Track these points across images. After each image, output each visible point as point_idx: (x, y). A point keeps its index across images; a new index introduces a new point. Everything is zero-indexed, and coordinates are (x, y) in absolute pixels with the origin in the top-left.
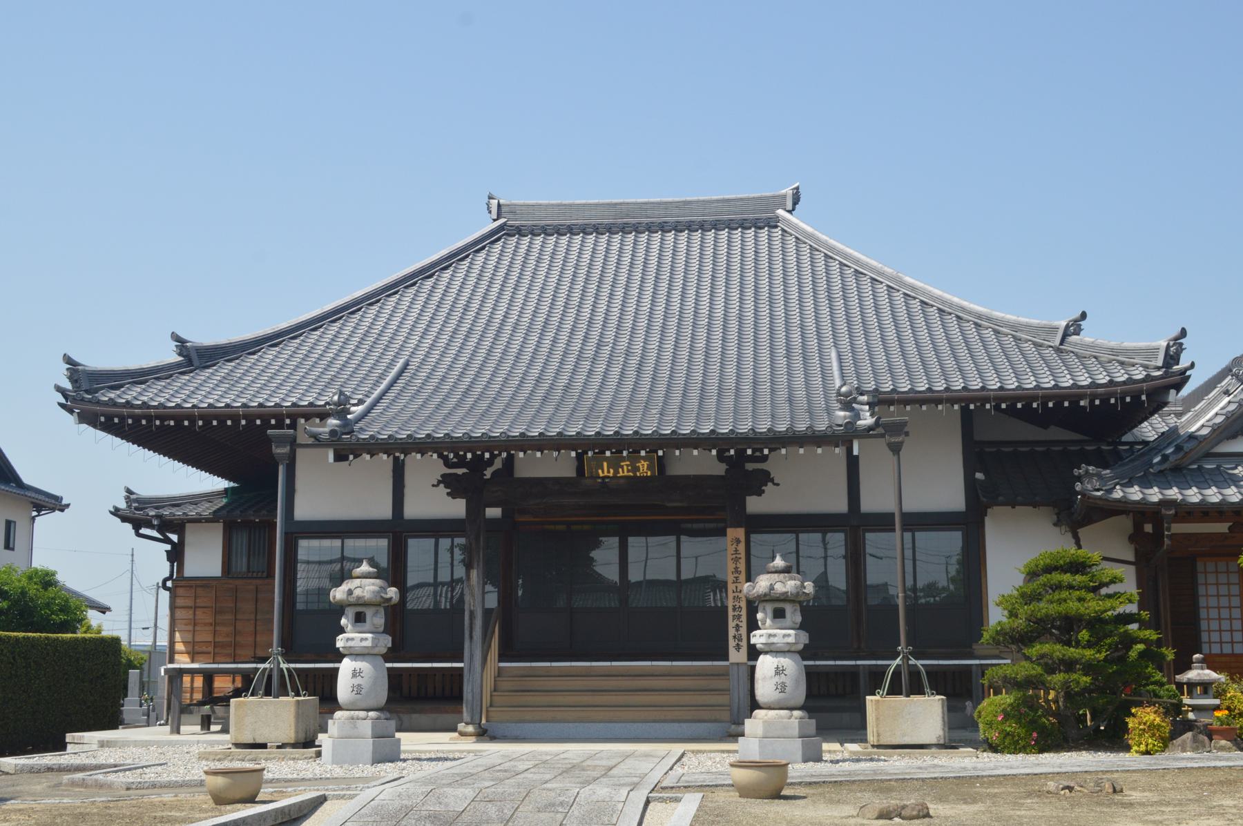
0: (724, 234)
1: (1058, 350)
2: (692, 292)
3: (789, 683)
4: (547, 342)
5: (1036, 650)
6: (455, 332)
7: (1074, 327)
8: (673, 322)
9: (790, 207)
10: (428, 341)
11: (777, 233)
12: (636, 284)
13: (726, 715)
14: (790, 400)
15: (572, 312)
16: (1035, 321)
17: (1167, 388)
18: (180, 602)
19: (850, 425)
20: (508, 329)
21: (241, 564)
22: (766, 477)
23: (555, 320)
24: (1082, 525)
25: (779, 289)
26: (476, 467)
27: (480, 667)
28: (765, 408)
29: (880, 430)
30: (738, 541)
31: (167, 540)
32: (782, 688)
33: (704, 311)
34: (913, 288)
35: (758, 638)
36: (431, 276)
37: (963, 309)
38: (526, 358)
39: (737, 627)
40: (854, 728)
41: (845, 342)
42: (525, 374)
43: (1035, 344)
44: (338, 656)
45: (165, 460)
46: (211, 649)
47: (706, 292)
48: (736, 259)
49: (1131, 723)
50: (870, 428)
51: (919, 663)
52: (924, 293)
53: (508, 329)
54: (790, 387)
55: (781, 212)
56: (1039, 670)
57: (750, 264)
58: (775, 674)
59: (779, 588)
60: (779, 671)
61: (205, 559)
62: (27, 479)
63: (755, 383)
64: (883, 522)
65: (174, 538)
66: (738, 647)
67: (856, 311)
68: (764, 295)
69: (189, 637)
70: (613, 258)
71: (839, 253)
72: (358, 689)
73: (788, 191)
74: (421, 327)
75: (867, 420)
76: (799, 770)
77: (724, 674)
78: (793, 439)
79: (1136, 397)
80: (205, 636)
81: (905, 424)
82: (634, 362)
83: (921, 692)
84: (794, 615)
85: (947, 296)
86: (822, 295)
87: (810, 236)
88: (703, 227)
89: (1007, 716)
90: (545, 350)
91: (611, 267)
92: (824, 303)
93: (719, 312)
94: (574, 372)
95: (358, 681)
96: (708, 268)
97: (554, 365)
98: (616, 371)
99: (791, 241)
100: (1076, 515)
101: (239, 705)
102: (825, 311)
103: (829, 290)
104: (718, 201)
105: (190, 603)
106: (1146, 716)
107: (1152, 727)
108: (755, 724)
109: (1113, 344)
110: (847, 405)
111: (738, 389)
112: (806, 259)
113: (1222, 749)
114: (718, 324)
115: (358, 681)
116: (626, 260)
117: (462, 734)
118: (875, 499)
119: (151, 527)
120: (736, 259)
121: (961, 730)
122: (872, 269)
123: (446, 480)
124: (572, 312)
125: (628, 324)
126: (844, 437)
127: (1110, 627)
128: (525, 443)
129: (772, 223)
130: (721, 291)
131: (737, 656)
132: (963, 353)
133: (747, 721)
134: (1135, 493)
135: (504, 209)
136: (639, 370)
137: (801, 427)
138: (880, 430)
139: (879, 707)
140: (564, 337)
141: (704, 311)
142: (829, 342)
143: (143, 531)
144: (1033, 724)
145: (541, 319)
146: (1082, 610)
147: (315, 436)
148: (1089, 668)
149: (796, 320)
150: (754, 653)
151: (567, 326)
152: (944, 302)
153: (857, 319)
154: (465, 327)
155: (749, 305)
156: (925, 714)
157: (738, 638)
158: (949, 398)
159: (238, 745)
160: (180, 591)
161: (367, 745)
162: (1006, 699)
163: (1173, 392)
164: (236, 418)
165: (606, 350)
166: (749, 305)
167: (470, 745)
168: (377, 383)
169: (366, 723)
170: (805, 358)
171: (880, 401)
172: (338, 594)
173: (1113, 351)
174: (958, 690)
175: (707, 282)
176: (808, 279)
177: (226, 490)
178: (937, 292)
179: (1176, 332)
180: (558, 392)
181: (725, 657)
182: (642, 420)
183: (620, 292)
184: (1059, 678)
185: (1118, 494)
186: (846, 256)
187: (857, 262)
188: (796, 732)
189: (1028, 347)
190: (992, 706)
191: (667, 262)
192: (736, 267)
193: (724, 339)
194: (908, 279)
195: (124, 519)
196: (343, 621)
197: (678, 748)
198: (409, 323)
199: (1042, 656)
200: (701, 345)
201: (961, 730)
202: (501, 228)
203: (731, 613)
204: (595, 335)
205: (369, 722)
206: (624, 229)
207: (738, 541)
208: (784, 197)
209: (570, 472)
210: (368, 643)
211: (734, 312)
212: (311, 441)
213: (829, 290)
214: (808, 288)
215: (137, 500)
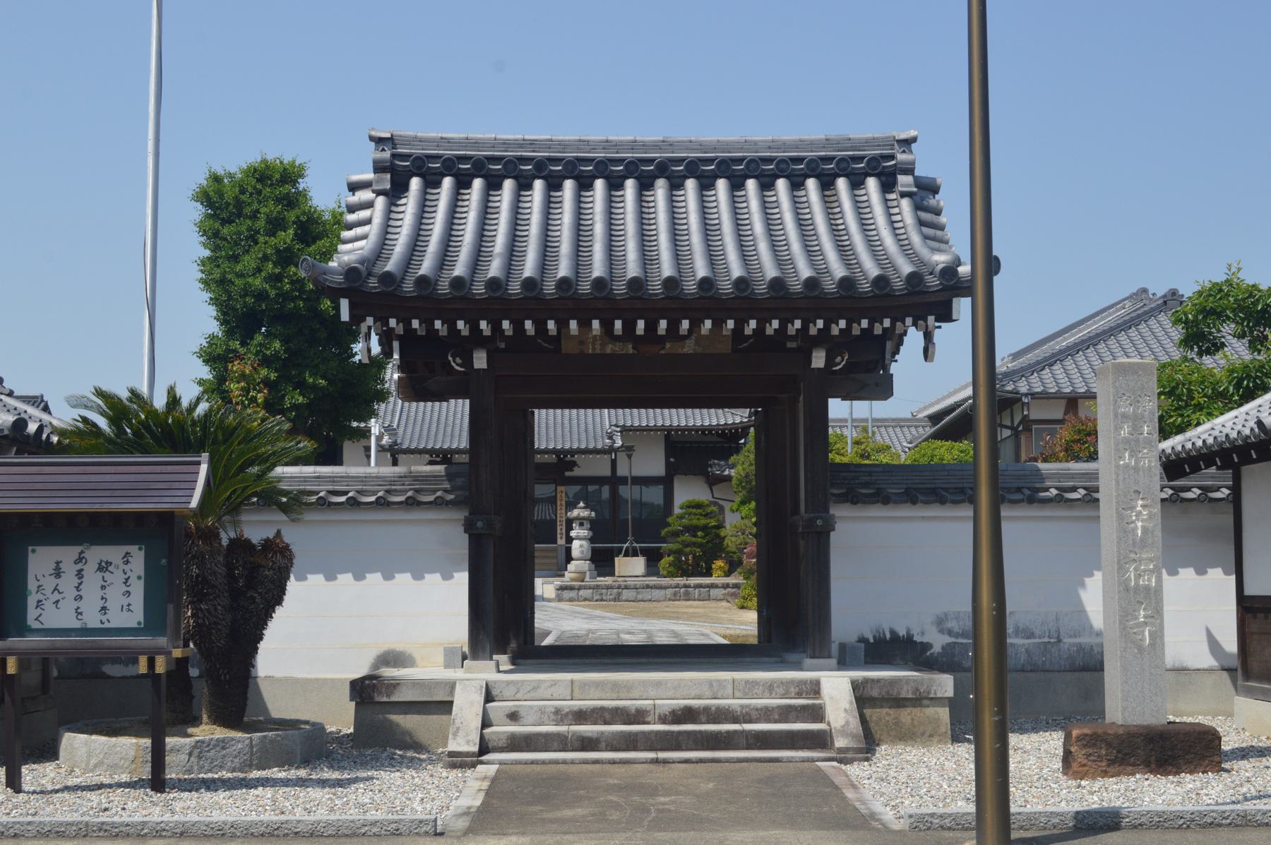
14: (586, 431)
19: (611, 447)
22: (574, 464)
28: (575, 436)
32: (582, 552)
64: (623, 480)
75: (619, 443)
76: (587, 579)
77: (555, 550)
79: (737, 430)
84: (587, 525)
100: (714, 481)
110: (610, 438)
118: (622, 471)
121: (652, 569)
126: (611, 450)
131: (561, 541)
137: (591, 446)
144: (679, 568)
148: (700, 545)
158: (656, 429)
174: (653, 559)
184: (688, 549)
185: (726, 473)
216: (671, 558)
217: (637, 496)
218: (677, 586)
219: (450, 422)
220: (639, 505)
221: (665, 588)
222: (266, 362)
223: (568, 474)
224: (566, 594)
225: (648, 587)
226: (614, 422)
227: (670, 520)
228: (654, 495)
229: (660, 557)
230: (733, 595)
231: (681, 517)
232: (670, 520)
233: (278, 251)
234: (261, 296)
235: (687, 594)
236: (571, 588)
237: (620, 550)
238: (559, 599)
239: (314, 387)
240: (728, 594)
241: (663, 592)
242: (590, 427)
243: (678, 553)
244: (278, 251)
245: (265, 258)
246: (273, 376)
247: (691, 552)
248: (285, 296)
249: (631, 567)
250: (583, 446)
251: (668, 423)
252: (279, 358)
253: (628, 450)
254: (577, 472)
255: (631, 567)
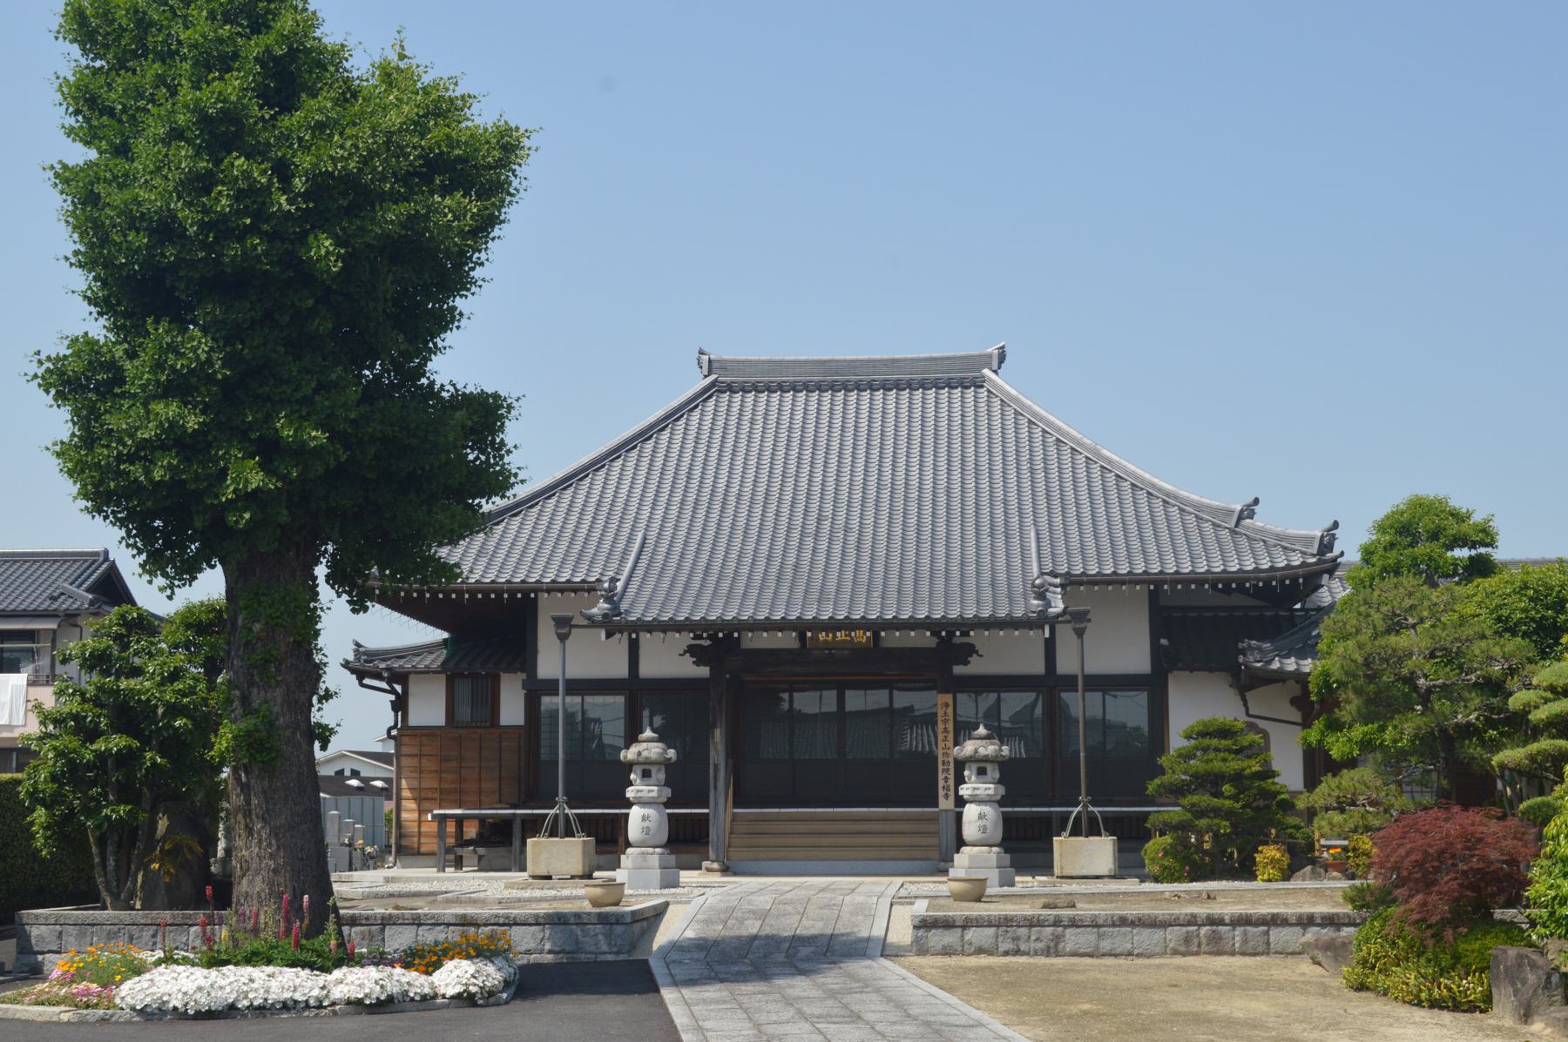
0: (931, 393)
1: (1233, 532)
2: (902, 460)
3: (989, 824)
4: (771, 515)
5: (1185, 801)
6: (683, 502)
7: (1248, 511)
8: (886, 494)
9: (995, 367)
10: (659, 513)
11: (983, 393)
12: (848, 451)
13: (935, 854)
14: (993, 584)
15: (790, 482)
16: (1215, 503)
17: (1320, 574)
18: (405, 750)
20: (732, 499)
21: (465, 712)
22: (970, 650)
23: (775, 489)
24: (1251, 688)
25: (984, 459)
26: (718, 643)
27: (721, 811)
29: (1068, 617)
30: (947, 705)
31: (393, 691)
32: (984, 829)
33: (914, 483)
34: (1110, 461)
35: (965, 791)
36: (649, 438)
37: (1154, 486)
38: (754, 532)
39: (946, 779)
40: (1046, 867)
41: (1043, 519)
42: (756, 550)
43: (1214, 524)
44: (629, 804)
45: (414, 622)
46: (436, 795)
47: (915, 460)
48: (944, 423)
49: (1258, 857)
50: (1058, 615)
51: (1095, 809)
52: (1120, 467)
53: (732, 499)
54: (993, 570)
55: (986, 372)
56: (1189, 815)
57: (957, 430)
58: (977, 819)
59: (982, 751)
60: (981, 816)
61: (429, 710)
62: (140, 604)
63: (962, 564)
64: (1069, 682)
65: (398, 688)
66: (947, 796)
67: (1055, 484)
68: (971, 466)
69: (415, 784)
70: (825, 420)
71: (1042, 419)
72: (647, 830)
73: (992, 350)
74: (650, 496)
75: (1058, 606)
76: (993, 889)
77: (934, 819)
78: (993, 624)
79: (1294, 580)
80: (430, 782)
81: (1086, 613)
82: (853, 538)
83: (1099, 834)
84: (993, 772)
85: (1140, 472)
86: (1025, 467)
87: (1016, 400)
88: (911, 386)
89: (1166, 853)
90: (769, 524)
91: (824, 431)
92: (1026, 475)
93: (928, 485)
94: (800, 549)
95: (647, 824)
96: (917, 433)
97: (780, 543)
98: (837, 547)
99: (996, 403)
100: (1247, 682)
101: (535, 844)
102: (1027, 484)
103: (1031, 460)
104: (925, 359)
105: (415, 751)
106: (1269, 853)
107: (1273, 860)
108: (963, 859)
109: (1279, 529)
110: (1041, 596)
111: (947, 571)
112: (1010, 424)
113: (1334, 878)
114: (928, 496)
115: (647, 824)
116: (838, 422)
117: (709, 870)
118: (1067, 664)
119: (378, 676)
120: (944, 423)
121: (1129, 865)
122: (1073, 439)
123: (692, 650)
124: (790, 482)
125: (844, 497)
127: (1247, 782)
128: (755, 626)
129: (978, 384)
130: (929, 460)
131: (946, 804)
132: (1149, 533)
133: (956, 856)
134: (1291, 664)
135: (715, 365)
136: (858, 549)
137: (1002, 613)
138: (1068, 617)
139: (1064, 847)
140: (785, 510)
141: (914, 483)
142: (1029, 520)
143: (367, 681)
144: (1186, 860)
145: (762, 488)
146: (1224, 769)
147: (589, 618)
148: (1228, 814)
149: (999, 494)
150: (961, 802)
151: (788, 498)
152: (1137, 477)
153: (1056, 494)
154: (691, 498)
155: (957, 476)
156: (1100, 852)
157: (946, 788)
158: (1132, 580)
159: (534, 877)
160: (405, 740)
161: (656, 874)
162: (1168, 839)
163: (1326, 577)
164: (499, 592)
165: (827, 524)
166: (957, 476)
167: (716, 878)
168: (623, 560)
169: (655, 857)
170: (1007, 536)
171: (1071, 583)
172: (630, 754)
173: (1280, 537)
174: (1130, 835)
175: (916, 450)
176: (1011, 448)
177: (445, 641)
178: (1132, 467)
179: (1329, 524)
180: (789, 571)
181: (936, 805)
182: (867, 604)
183: (834, 460)
184: (1203, 822)
185: (1275, 665)
186: (1049, 423)
187: (1058, 430)
188: (994, 863)
189: (1207, 527)
190: (1155, 846)
191: (877, 425)
192: (944, 432)
193: (934, 515)
194: (1105, 452)
195: (353, 671)
196: (632, 776)
197: (900, 880)
198: (638, 491)
199: (1193, 805)
200: (913, 521)
201: (1129, 865)
202: (713, 384)
203: (940, 767)
204: (814, 507)
205: (656, 857)
206: (833, 388)
207: (947, 705)
208: (990, 356)
209: (795, 645)
210: (654, 794)
211: (942, 484)
212: (586, 622)
213: (1031, 460)
214: (1012, 458)
215: (365, 653)
216: (1168, 839)
217: (1095, 710)
218: (1192, 921)
219: (730, 571)
220: (1102, 726)
221: (1164, 924)
222: (178, 387)
223: (958, 670)
224: (937, 938)
225: (1123, 922)
226: (1049, 567)
227: (1163, 761)
228: (1130, 710)
229: (1146, 836)
230: (1329, 946)
231: (1186, 756)
232: (1163, 761)
233: (204, 120)
234: (165, 229)
235: (1215, 939)
236: (947, 924)
237: (1064, 818)
238: (921, 949)
239: (300, 452)
240: (1317, 945)
241: (1158, 934)
242: (1002, 576)
243: (1182, 827)
244: (204, 120)
245: (176, 134)
246: (192, 422)
247: (1209, 829)
248: (221, 228)
249: (1087, 855)
250: (986, 614)
251: (1155, 568)
252: (211, 379)
253: (1077, 619)
254: (975, 667)
255: (1087, 855)
